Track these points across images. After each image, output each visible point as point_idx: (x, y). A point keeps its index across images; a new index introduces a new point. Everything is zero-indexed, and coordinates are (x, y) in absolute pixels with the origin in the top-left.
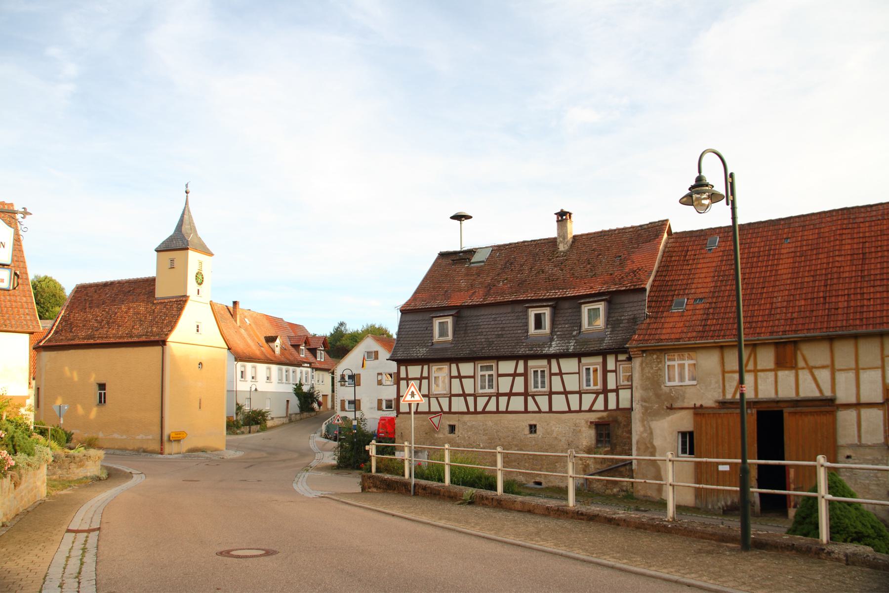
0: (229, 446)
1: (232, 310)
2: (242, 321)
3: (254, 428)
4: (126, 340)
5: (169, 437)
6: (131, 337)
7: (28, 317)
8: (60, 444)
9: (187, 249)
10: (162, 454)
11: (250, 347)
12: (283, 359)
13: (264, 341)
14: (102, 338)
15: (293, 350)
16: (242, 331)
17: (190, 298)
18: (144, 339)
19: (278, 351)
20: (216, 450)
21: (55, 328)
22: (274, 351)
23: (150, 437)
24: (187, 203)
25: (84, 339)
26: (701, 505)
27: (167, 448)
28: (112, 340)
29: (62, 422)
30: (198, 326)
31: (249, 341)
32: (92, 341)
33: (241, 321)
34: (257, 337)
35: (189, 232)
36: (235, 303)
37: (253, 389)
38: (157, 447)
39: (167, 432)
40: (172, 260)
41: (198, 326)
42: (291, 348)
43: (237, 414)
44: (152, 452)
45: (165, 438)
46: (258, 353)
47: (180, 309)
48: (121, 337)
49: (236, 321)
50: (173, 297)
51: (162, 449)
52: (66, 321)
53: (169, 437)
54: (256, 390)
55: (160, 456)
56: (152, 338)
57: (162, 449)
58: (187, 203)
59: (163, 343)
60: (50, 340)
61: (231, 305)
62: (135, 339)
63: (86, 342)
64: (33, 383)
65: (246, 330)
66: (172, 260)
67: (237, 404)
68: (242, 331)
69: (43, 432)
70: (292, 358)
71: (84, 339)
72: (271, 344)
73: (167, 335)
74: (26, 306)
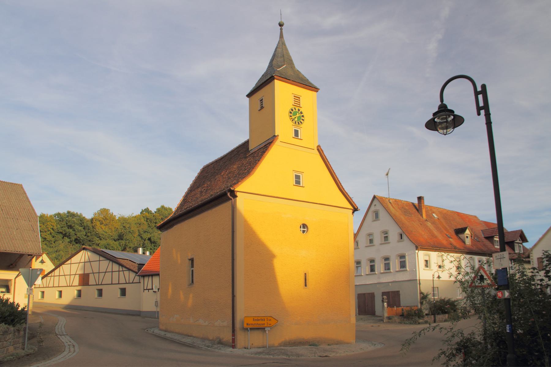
0: (361, 336)
1: (417, 207)
2: (429, 216)
3: (439, 317)
10: (234, 347)
11: (436, 237)
12: (475, 249)
13: (453, 233)
15: (487, 242)
16: (429, 224)
17: (280, 139)
19: (468, 242)
20: (339, 343)
22: (464, 242)
24: (281, 36)
27: (241, 337)
31: (436, 232)
33: (427, 215)
34: (446, 229)
36: (420, 199)
37: (436, 276)
38: (227, 336)
39: (239, 316)
42: (484, 240)
43: (422, 303)
44: (221, 343)
45: (238, 325)
46: (445, 242)
49: (422, 215)
51: (234, 340)
53: (243, 322)
54: (439, 277)
55: (229, 350)
57: (234, 340)
58: (281, 36)
61: (416, 202)
65: (433, 223)
67: (421, 293)
68: (429, 224)
70: (484, 249)
72: (461, 236)
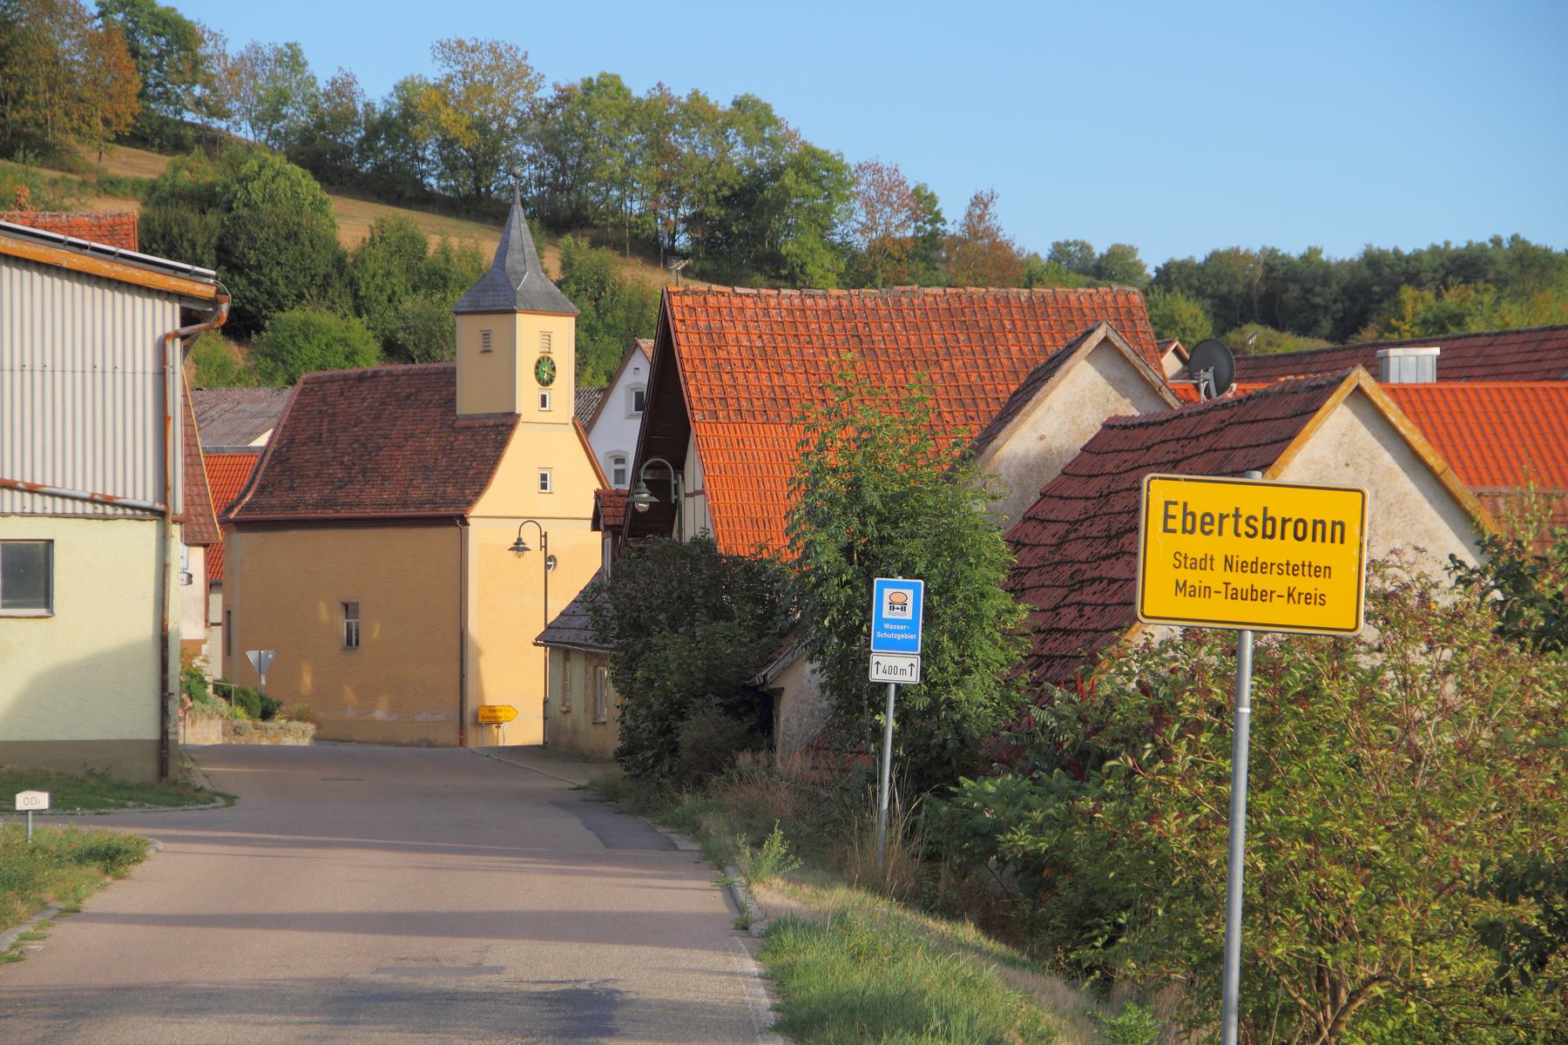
4: (394, 513)
5: (476, 716)
6: (405, 505)
7: (202, 520)
8: (249, 711)
9: (514, 312)
14: (350, 505)
17: (523, 418)
18: (427, 511)
21: (259, 477)
23: (441, 717)
25: (316, 506)
26: (558, 747)
28: (370, 512)
29: (263, 682)
30: (544, 477)
32: (330, 514)
35: (520, 268)
38: (451, 735)
40: (486, 335)
41: (544, 477)
45: (469, 719)
47: (502, 444)
48: (387, 505)
50: (488, 416)
52: (281, 462)
56: (443, 511)
59: (464, 521)
60: (248, 508)
62: (411, 512)
63: (319, 514)
64: (217, 600)
66: (486, 335)
69: (226, 695)
71: (316, 506)
73: (470, 504)
74: (197, 500)
